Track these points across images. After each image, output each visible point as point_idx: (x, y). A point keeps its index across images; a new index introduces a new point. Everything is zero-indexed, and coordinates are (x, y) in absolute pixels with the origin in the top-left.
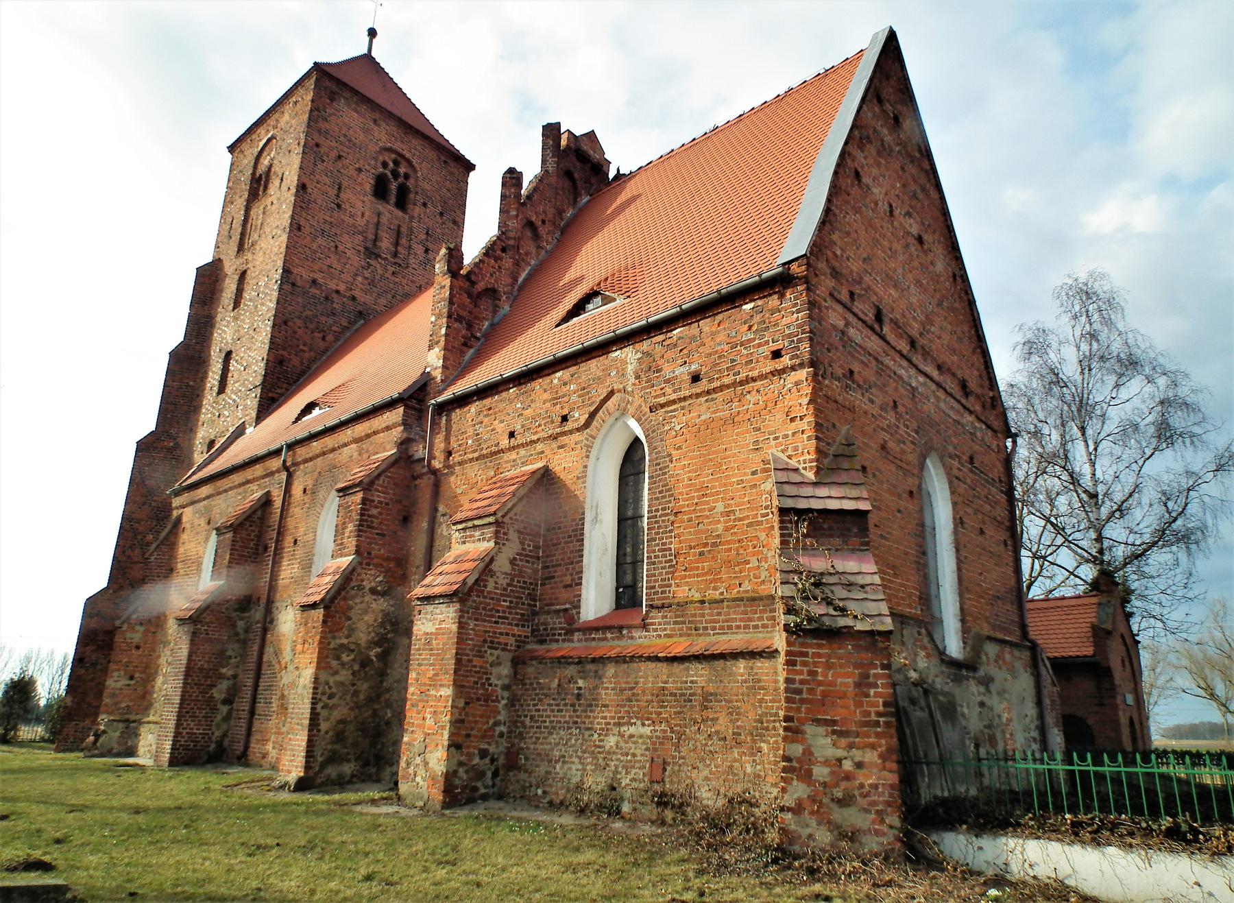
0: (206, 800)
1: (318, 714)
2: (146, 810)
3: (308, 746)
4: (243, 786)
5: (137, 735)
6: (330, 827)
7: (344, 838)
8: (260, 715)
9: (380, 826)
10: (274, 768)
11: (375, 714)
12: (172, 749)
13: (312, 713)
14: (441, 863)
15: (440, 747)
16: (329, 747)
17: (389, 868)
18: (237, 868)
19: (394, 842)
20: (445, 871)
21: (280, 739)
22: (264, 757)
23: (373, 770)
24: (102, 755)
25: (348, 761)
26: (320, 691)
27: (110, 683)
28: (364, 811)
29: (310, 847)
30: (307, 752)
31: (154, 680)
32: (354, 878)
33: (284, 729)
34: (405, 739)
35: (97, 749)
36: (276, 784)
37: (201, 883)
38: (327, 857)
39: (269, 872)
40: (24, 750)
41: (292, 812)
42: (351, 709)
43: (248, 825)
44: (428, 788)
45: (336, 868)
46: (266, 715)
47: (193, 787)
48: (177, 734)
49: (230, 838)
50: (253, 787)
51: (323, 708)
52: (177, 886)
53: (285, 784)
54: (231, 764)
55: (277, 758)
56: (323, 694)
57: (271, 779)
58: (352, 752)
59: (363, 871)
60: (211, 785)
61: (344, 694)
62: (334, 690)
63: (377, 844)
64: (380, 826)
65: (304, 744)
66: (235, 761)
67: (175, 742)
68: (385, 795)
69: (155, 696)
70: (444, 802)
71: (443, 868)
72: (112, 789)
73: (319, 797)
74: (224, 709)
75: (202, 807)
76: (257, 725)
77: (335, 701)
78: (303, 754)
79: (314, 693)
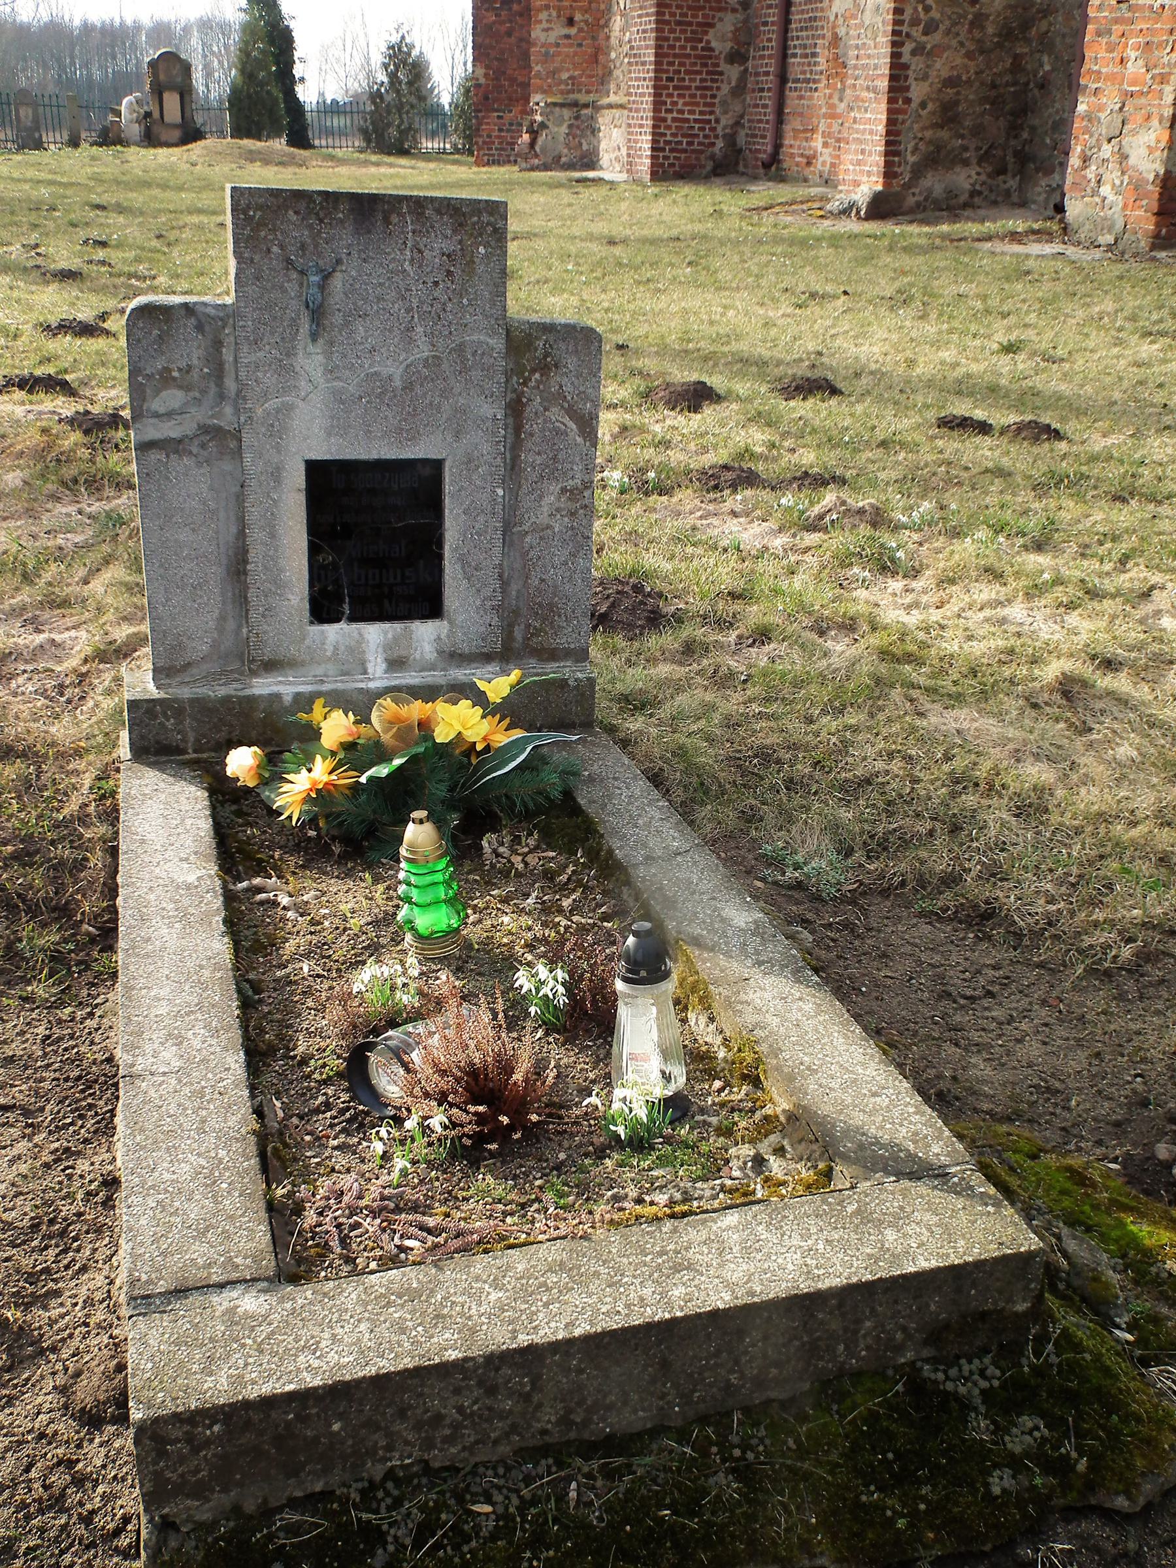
0: (720, 230)
1: (906, 67)
2: (625, 241)
3: (888, 133)
4: (777, 209)
5: (594, 131)
6: (934, 272)
7: (962, 289)
8: (797, 81)
9: (1028, 273)
10: (828, 182)
11: (1017, 66)
12: (653, 149)
13: (893, 66)
14: (1151, 334)
15: (1155, 122)
16: (928, 134)
17: (1050, 334)
18: (780, 322)
19: (1056, 297)
20: (1156, 346)
21: (836, 127)
22: (809, 164)
23: (1013, 183)
24: (546, 167)
25: (966, 163)
26: (907, 16)
27: (537, 33)
28: (998, 250)
29: (902, 299)
30: (888, 143)
31: (606, 25)
32: (983, 348)
33: (842, 107)
34: (1081, 108)
35: (536, 156)
36: (833, 206)
37: (727, 339)
38: (933, 316)
39: (833, 332)
40: (432, 165)
41: (867, 246)
42: (969, 55)
43: (792, 265)
44: (1125, 206)
45: (950, 331)
46: (808, 81)
47: (695, 209)
48: (658, 121)
49: (763, 282)
50: (794, 211)
51: (914, 53)
52: (689, 341)
53: (851, 207)
54: (755, 178)
55: (833, 165)
56: (915, 22)
57: (824, 199)
58: (972, 146)
59: (1001, 337)
60: (725, 208)
61: (955, 24)
62: (935, 14)
63: (1024, 301)
64: (1028, 273)
65: (881, 128)
66: (761, 171)
67: (656, 135)
68: (1036, 226)
69: (613, 55)
70: (1157, 236)
71: (1152, 342)
72: (568, 211)
73: (914, 229)
74: (733, 72)
75: (712, 238)
76: (792, 101)
77: (937, 38)
78: (881, 148)
79: (896, 22)
